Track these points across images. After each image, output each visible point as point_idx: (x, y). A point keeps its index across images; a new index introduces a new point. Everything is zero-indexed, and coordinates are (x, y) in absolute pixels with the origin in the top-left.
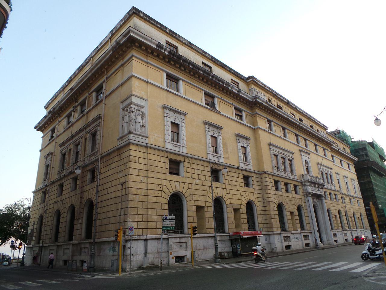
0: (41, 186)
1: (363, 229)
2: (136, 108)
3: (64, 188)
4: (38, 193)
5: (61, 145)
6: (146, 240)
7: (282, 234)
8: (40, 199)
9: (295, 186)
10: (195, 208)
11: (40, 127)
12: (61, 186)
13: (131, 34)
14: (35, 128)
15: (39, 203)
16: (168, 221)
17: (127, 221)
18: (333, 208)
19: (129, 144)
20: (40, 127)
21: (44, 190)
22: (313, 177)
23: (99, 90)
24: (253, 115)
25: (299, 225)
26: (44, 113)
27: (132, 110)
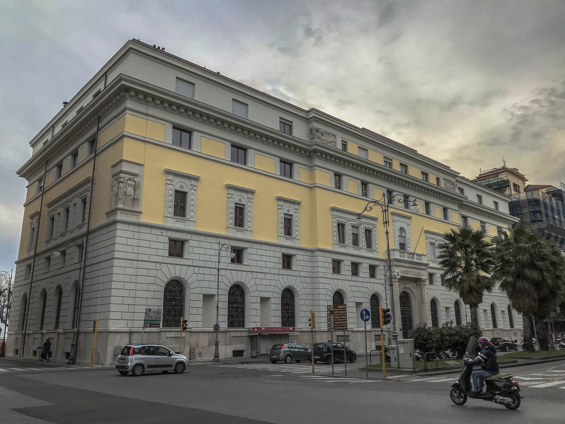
0: (25, 256)
1: (382, 336)
2: (127, 177)
3: (52, 263)
4: (22, 264)
5: (49, 205)
6: (131, 333)
7: (162, 333)
8: (24, 273)
9: (372, 268)
10: (201, 297)
11: (26, 172)
12: (48, 259)
13: (123, 82)
14: (18, 173)
15: (23, 277)
16: (152, 314)
17: (316, 278)
18: (503, 298)
19: (115, 222)
20: (26, 172)
21: (31, 261)
22: (415, 256)
23: (93, 141)
24: (310, 167)
25: (491, 322)
26: (30, 153)
27: (122, 180)
